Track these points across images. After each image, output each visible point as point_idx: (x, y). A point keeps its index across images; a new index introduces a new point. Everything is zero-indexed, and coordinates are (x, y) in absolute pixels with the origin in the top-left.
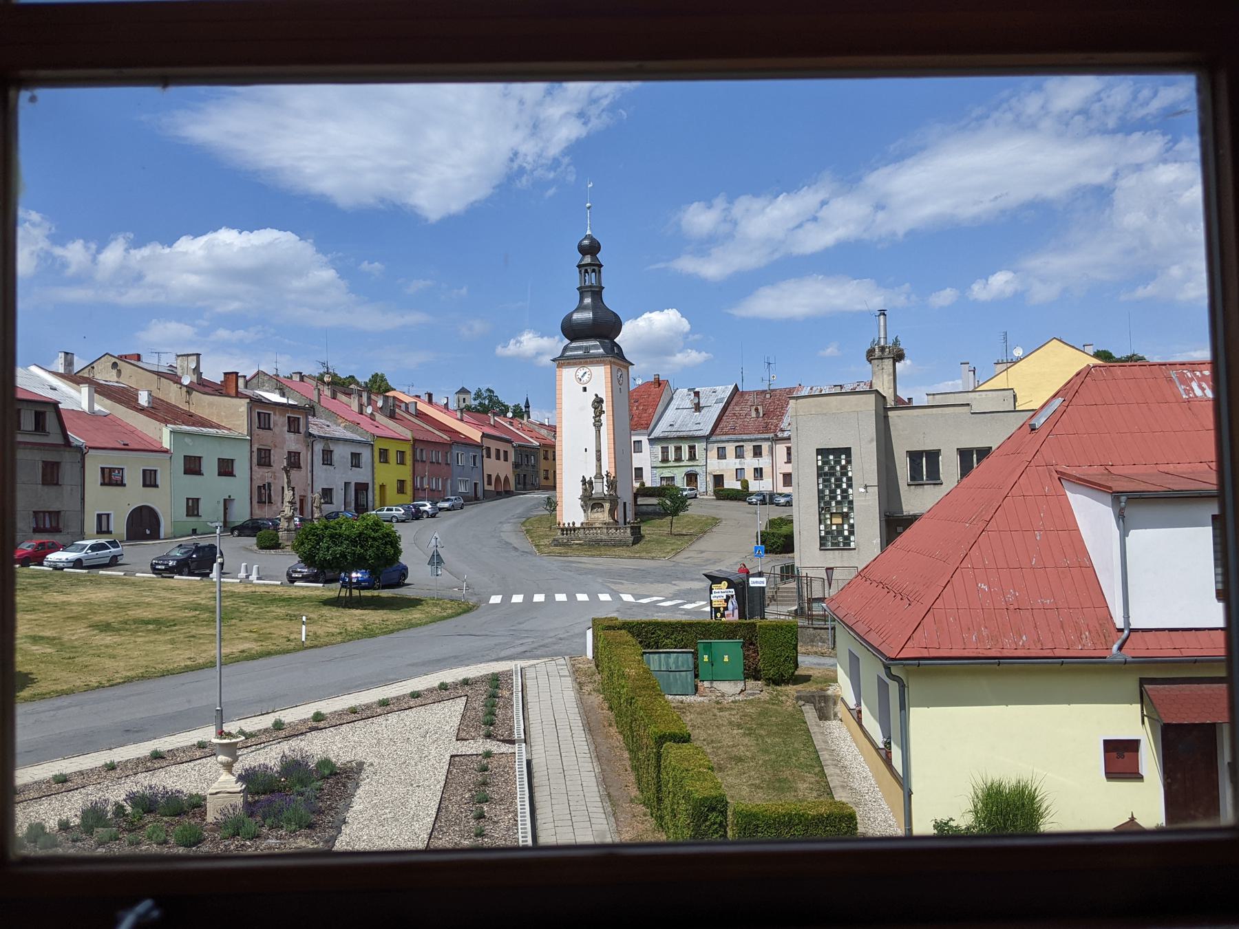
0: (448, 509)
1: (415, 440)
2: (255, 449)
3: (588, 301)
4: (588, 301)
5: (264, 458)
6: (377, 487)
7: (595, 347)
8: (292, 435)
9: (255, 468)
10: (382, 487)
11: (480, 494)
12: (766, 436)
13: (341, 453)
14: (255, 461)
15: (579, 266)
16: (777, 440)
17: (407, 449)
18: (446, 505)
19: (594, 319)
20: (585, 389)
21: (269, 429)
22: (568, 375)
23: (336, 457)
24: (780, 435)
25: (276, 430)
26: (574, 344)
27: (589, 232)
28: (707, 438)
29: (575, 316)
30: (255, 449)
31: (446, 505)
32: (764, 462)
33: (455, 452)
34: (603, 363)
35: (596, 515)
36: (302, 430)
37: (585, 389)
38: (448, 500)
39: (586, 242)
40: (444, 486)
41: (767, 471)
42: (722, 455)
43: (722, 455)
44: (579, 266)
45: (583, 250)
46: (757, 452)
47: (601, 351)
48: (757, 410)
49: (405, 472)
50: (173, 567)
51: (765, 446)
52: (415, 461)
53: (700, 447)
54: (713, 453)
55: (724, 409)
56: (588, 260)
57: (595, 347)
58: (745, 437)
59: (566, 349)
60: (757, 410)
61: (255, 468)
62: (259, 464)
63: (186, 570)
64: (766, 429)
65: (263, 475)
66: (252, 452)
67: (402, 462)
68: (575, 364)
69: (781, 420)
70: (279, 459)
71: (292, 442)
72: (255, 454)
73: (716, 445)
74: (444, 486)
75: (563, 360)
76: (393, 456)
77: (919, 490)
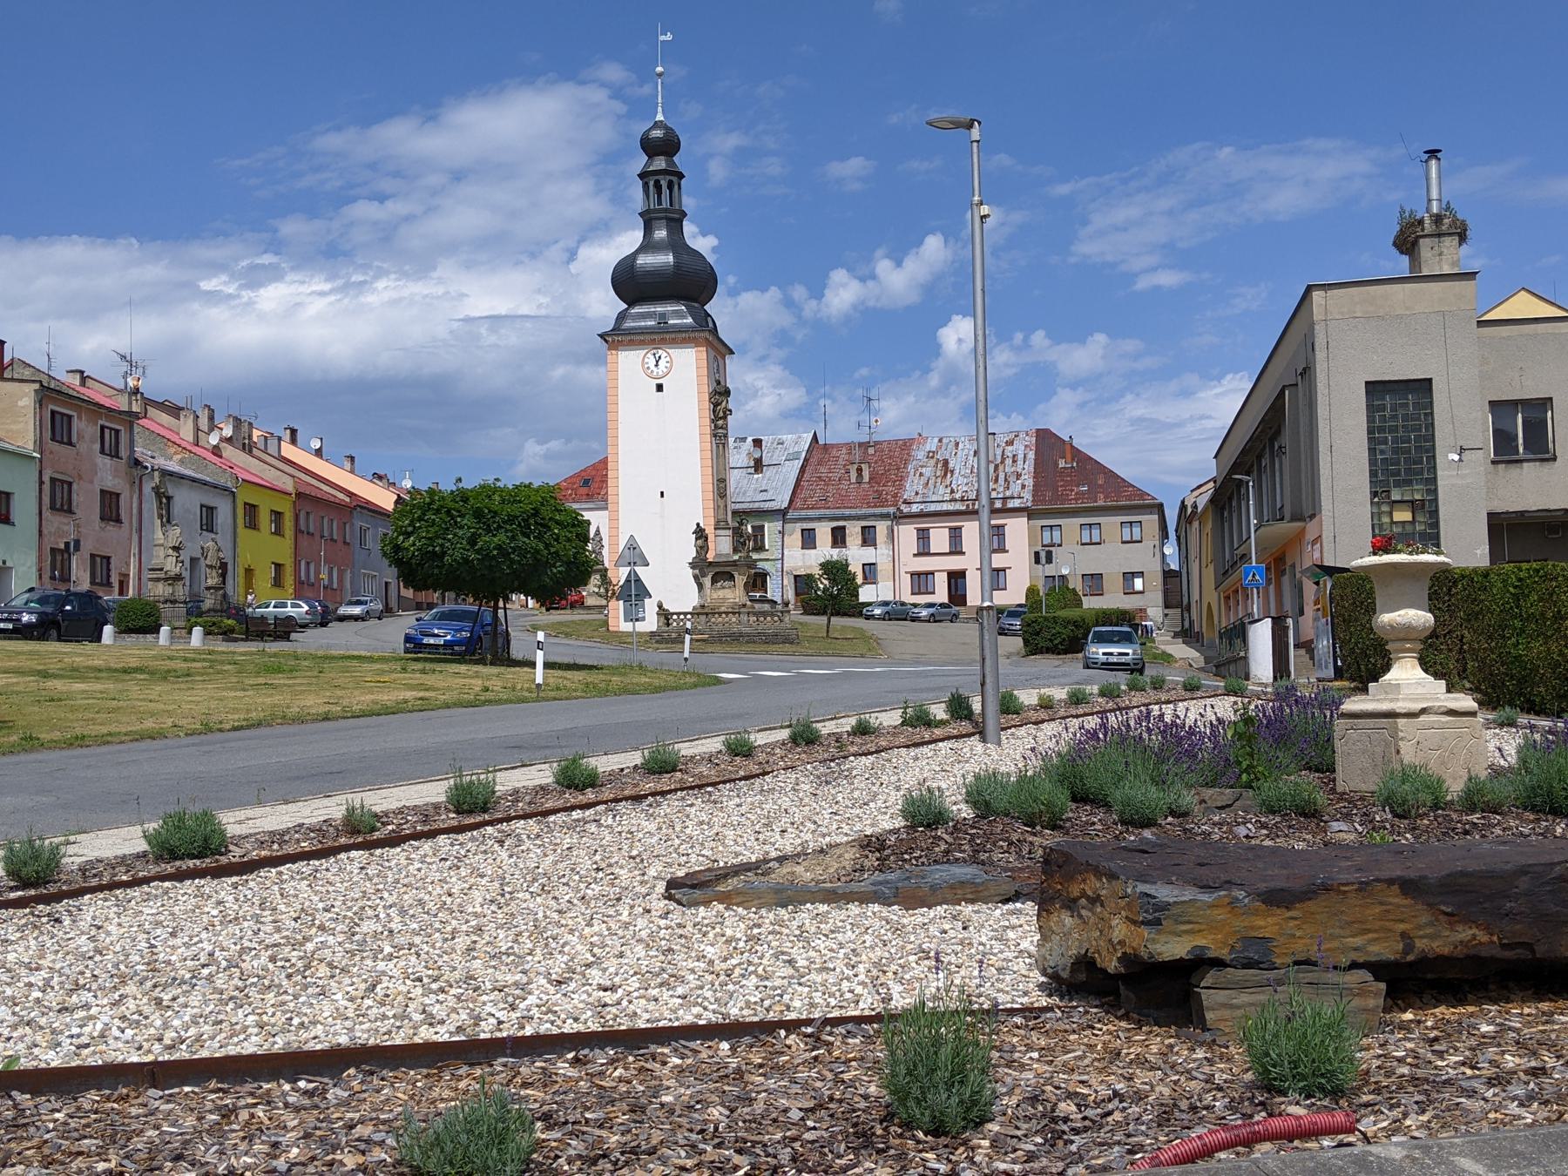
0: (356, 618)
1: (299, 495)
2: (46, 479)
3: (661, 234)
4: (661, 234)
5: (59, 497)
6: (241, 572)
7: (677, 314)
8: (107, 460)
9: (47, 513)
10: (249, 572)
11: (393, 603)
12: (884, 510)
13: (186, 501)
14: (46, 500)
15: (642, 176)
16: (900, 518)
17: (286, 507)
18: (357, 610)
19: (677, 265)
20: (660, 388)
21: (70, 443)
22: (630, 363)
23: (177, 508)
24: (905, 509)
25: (82, 447)
26: (636, 310)
27: (660, 117)
28: (782, 514)
29: (642, 260)
30: (46, 479)
31: (357, 610)
32: (879, 555)
33: (358, 523)
34: (695, 342)
35: (721, 593)
36: (123, 453)
37: (660, 388)
38: (359, 603)
39: (657, 133)
40: (341, 580)
41: (884, 566)
42: (809, 540)
43: (809, 540)
44: (642, 176)
45: (650, 147)
46: (868, 538)
47: (690, 320)
48: (860, 470)
49: (282, 549)
50: (29, 625)
51: (882, 527)
52: (298, 531)
53: (771, 529)
54: (795, 539)
55: (803, 470)
56: (660, 163)
57: (678, 314)
58: (847, 512)
59: (622, 317)
60: (860, 470)
61: (47, 513)
62: (53, 507)
63: (54, 633)
64: (880, 500)
65: (61, 529)
66: (41, 483)
67: (278, 532)
68: (641, 344)
69: (901, 487)
70: (86, 503)
71: (108, 474)
72: (47, 487)
73: (799, 526)
74: (341, 580)
75: (618, 337)
76: (264, 518)
77: (1514, 471)
